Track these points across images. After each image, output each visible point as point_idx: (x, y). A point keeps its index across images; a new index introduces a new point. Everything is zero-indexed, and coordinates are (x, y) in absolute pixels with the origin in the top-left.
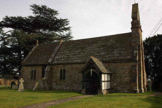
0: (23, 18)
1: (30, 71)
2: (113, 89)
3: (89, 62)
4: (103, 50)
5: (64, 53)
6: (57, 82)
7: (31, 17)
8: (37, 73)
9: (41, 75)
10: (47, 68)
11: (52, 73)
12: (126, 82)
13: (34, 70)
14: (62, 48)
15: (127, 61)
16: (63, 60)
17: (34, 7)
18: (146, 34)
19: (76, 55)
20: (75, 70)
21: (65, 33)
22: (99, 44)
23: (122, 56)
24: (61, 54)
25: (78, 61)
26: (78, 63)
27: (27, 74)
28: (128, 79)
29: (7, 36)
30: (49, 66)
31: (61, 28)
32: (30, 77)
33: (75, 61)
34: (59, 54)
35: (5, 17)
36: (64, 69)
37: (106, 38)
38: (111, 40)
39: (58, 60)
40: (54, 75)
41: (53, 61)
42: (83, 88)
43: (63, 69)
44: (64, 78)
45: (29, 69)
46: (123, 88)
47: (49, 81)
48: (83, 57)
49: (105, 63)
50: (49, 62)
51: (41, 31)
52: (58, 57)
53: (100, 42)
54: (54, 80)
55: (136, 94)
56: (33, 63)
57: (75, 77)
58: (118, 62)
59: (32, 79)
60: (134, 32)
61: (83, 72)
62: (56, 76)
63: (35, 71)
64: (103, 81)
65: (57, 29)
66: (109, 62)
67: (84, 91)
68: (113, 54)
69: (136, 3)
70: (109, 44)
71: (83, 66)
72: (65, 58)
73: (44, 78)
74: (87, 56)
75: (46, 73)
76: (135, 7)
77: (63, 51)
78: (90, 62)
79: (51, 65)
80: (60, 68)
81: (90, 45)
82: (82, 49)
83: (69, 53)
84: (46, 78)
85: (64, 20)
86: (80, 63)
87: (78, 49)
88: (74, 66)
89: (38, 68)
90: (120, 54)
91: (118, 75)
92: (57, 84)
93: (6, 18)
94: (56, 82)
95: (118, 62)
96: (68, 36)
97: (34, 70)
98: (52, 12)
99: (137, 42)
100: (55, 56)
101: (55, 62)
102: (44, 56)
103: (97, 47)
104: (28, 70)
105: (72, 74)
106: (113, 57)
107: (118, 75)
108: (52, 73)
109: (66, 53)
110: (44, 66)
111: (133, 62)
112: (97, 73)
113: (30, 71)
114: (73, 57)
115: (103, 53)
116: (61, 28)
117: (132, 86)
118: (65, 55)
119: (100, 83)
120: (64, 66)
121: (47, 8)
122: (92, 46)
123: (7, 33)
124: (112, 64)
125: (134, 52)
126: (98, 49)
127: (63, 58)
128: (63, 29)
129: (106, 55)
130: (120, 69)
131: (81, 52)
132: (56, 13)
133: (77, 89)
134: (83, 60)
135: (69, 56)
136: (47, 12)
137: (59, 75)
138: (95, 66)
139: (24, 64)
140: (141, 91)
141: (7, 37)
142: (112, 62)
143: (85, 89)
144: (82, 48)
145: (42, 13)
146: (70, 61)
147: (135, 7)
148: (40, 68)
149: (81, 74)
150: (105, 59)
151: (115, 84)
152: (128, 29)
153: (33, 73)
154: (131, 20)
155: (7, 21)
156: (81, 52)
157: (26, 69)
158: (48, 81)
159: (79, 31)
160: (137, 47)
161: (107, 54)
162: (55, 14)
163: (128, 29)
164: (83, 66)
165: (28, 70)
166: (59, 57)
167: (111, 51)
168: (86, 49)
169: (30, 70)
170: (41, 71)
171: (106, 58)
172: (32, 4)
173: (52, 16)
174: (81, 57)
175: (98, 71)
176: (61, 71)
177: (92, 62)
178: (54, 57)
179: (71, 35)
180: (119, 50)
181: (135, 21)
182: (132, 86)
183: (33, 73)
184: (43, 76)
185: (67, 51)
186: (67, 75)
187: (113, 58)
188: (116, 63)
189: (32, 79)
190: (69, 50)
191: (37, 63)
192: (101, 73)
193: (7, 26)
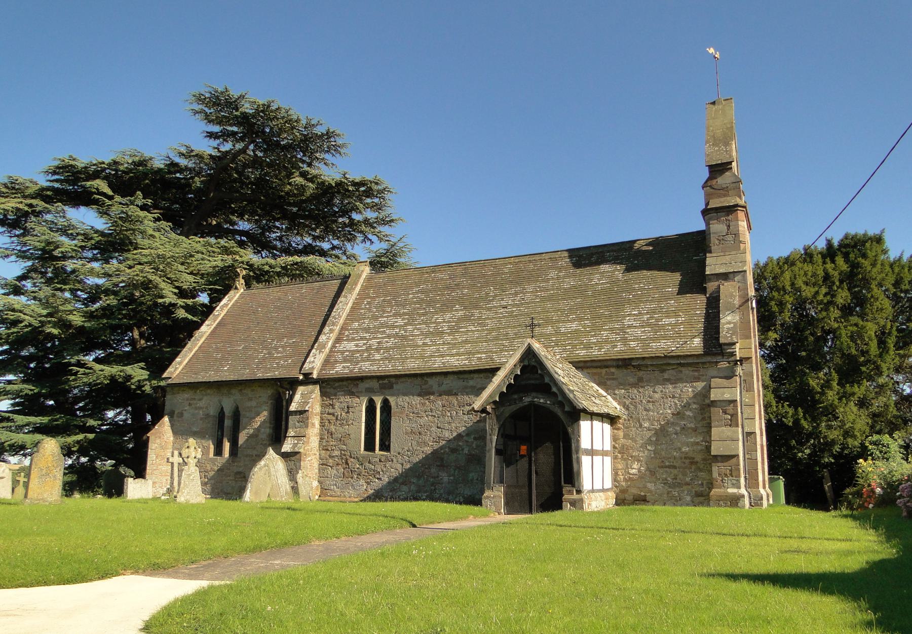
1: (207, 416)
5: (382, 325)
7: (188, 154)
10: (297, 397)
12: (685, 458)
14: (369, 303)
16: (377, 357)
19: (441, 333)
23: (665, 337)
24: (367, 330)
26: (453, 373)
28: (697, 443)
34: (357, 331)
37: (580, 256)
39: (350, 358)
52: (351, 346)
63: (386, 408)
64: (604, 453)
65: (194, 297)
72: (387, 349)
83: (406, 324)
86: (464, 372)
87: (447, 307)
89: (250, 399)
98: (312, 143)
102: (280, 340)
103: (543, 300)
106: (625, 340)
109: (393, 327)
113: (207, 416)
115: (574, 326)
118: (389, 337)
119: (574, 456)
122: (516, 294)
134: (480, 358)
135: (404, 338)
138: (547, 380)
140: (756, 502)
150: (583, 352)
153: (228, 423)
156: (467, 318)
157: (190, 405)
165: (200, 408)
166: (357, 346)
168: (489, 309)
169: (213, 411)
171: (588, 347)
175: (561, 405)
180: (652, 312)
183: (228, 423)
185: (395, 315)
187: (620, 347)
190: (404, 314)
191: (246, 374)
192: (576, 414)
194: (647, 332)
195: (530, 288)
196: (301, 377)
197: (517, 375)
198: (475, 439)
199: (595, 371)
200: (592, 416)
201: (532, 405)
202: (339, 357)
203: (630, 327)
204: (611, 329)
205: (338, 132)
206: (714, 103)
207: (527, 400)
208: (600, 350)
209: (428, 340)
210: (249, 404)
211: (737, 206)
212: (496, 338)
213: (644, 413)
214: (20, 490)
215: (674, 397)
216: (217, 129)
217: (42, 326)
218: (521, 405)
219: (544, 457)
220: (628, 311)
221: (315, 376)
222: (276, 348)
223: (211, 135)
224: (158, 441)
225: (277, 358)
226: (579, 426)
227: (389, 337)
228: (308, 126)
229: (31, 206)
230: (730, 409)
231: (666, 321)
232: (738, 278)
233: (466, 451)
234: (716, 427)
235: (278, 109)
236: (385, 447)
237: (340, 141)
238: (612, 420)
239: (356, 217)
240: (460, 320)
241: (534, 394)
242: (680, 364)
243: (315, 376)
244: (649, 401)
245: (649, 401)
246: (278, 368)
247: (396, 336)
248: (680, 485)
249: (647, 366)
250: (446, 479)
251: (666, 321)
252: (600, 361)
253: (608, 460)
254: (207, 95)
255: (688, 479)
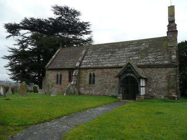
0: (19, 25)
2: (148, 95)
3: (126, 66)
4: (136, 54)
5: (92, 57)
6: (86, 87)
8: (63, 77)
9: (67, 79)
10: (74, 72)
11: (80, 77)
13: (59, 74)
14: (89, 52)
15: (151, 66)
16: (92, 64)
17: (55, 8)
18: (180, 39)
19: (106, 59)
20: (106, 74)
21: (85, 37)
22: (130, 48)
23: (157, 61)
24: (89, 58)
25: (109, 65)
26: (108, 68)
27: (52, 78)
28: (166, 85)
29: (27, 38)
30: (77, 70)
31: (82, 32)
32: (55, 81)
33: (105, 65)
35: (24, 19)
36: (94, 73)
38: (143, 44)
39: (86, 64)
40: (82, 79)
41: (80, 65)
42: (119, 93)
43: (92, 73)
44: (94, 83)
45: (54, 73)
46: (159, 94)
47: (77, 85)
48: (114, 61)
49: (140, 67)
50: (76, 66)
51: (60, 34)
52: (86, 61)
53: (131, 46)
54: (83, 85)
55: (174, 101)
56: (59, 66)
57: (106, 82)
58: (154, 67)
59: (57, 84)
60: (171, 36)
61: (119, 76)
62: (85, 81)
63: (61, 75)
65: (77, 33)
66: (145, 67)
67: (120, 97)
68: (148, 58)
69: (172, 5)
70: (142, 48)
71: (119, 71)
72: (94, 62)
73: (72, 83)
74: (119, 60)
75: (74, 77)
76: (171, 10)
77: (91, 55)
78: (128, 66)
79: (79, 68)
80: (89, 73)
81: (120, 49)
82: (111, 53)
83: (98, 57)
84: (74, 83)
85: (87, 23)
87: (107, 53)
88: (105, 70)
89: (64, 72)
90: (156, 58)
91: (153, 80)
92: (85, 89)
93: (25, 20)
94: (85, 87)
95: (154, 67)
96: (90, 40)
97: (59, 74)
98: (75, 13)
99: (174, 47)
100: (83, 60)
101: (83, 66)
104: (53, 74)
105: (102, 78)
106: (149, 61)
107: (153, 80)
108: (80, 77)
110: (71, 70)
111: (171, 67)
112: (136, 78)
114: (103, 61)
115: (137, 58)
116: (82, 32)
117: (170, 92)
118: (94, 59)
120: (93, 71)
121: (70, 9)
122: (123, 50)
123: (24, 34)
124: (148, 69)
125: (172, 57)
126: (130, 53)
127: (92, 62)
128: (84, 33)
129: (140, 60)
130: (156, 74)
131: (112, 56)
132: (78, 14)
133: (108, 94)
134: (115, 65)
136: (69, 13)
137: (87, 80)
139: (48, 68)
141: (27, 40)
142: (147, 67)
143: (121, 95)
144: (113, 52)
145: (64, 15)
146: (100, 66)
147: (171, 10)
148: (67, 73)
149: (117, 79)
150: (139, 64)
151: (151, 90)
152: (162, 32)
153: (59, 77)
154: (168, 23)
155: (26, 23)
156: (112, 56)
158: (76, 85)
159: (101, 34)
160: (174, 52)
161: (141, 58)
162: (78, 15)
163: (162, 32)
164: (119, 71)
167: (145, 56)
170: (67, 75)
171: (140, 62)
172: (54, 5)
173: (74, 18)
174: (112, 61)
176: (90, 75)
177: (130, 66)
178: (82, 61)
179: (92, 39)
180: (155, 55)
181: (172, 25)
182: (170, 92)
183: (59, 77)
184: (70, 81)
186: (96, 79)
187: (148, 63)
188: (152, 68)
189: (57, 84)
190: (98, 54)
193: (25, 28)
194: (154, 60)
195: (126, 49)
198: (114, 82)
200: (143, 78)
201: (129, 76)
202: (83, 63)
203: (150, 58)
204: (145, 59)
207: (128, 75)
208: (143, 63)
209: (103, 60)
210: (64, 73)
212: (119, 60)
214: (74, 127)
217: (23, 47)
218: (126, 76)
220: (149, 54)
222: (69, 61)
225: (70, 64)
227: (94, 59)
231: (159, 57)
233: (112, 85)
236: (61, 83)
240: (110, 56)
241: (130, 73)
246: (70, 66)
247: (96, 59)
248: (161, 94)
250: (107, 91)
251: (159, 57)
255: (163, 93)
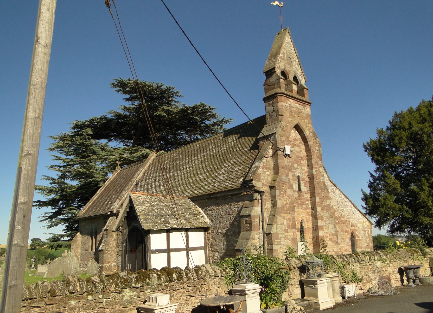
196: (109, 213)
197: (127, 212)
199: (199, 202)
205: (171, 87)
206: (279, 34)
211: (276, 94)
213: (219, 224)
215: (230, 214)
216: (128, 96)
219: (139, 255)
221: (114, 212)
223: (127, 100)
224: (75, 245)
226: (150, 238)
228: (159, 87)
229: (67, 144)
230: (248, 219)
232: (272, 138)
234: (243, 231)
235: (141, 82)
237: (175, 91)
238: (205, 230)
239: (207, 122)
242: (232, 195)
243: (114, 212)
244: (220, 217)
245: (220, 217)
249: (219, 197)
252: (202, 196)
253: (203, 252)
254: (116, 83)
